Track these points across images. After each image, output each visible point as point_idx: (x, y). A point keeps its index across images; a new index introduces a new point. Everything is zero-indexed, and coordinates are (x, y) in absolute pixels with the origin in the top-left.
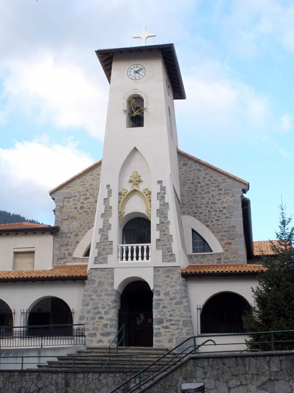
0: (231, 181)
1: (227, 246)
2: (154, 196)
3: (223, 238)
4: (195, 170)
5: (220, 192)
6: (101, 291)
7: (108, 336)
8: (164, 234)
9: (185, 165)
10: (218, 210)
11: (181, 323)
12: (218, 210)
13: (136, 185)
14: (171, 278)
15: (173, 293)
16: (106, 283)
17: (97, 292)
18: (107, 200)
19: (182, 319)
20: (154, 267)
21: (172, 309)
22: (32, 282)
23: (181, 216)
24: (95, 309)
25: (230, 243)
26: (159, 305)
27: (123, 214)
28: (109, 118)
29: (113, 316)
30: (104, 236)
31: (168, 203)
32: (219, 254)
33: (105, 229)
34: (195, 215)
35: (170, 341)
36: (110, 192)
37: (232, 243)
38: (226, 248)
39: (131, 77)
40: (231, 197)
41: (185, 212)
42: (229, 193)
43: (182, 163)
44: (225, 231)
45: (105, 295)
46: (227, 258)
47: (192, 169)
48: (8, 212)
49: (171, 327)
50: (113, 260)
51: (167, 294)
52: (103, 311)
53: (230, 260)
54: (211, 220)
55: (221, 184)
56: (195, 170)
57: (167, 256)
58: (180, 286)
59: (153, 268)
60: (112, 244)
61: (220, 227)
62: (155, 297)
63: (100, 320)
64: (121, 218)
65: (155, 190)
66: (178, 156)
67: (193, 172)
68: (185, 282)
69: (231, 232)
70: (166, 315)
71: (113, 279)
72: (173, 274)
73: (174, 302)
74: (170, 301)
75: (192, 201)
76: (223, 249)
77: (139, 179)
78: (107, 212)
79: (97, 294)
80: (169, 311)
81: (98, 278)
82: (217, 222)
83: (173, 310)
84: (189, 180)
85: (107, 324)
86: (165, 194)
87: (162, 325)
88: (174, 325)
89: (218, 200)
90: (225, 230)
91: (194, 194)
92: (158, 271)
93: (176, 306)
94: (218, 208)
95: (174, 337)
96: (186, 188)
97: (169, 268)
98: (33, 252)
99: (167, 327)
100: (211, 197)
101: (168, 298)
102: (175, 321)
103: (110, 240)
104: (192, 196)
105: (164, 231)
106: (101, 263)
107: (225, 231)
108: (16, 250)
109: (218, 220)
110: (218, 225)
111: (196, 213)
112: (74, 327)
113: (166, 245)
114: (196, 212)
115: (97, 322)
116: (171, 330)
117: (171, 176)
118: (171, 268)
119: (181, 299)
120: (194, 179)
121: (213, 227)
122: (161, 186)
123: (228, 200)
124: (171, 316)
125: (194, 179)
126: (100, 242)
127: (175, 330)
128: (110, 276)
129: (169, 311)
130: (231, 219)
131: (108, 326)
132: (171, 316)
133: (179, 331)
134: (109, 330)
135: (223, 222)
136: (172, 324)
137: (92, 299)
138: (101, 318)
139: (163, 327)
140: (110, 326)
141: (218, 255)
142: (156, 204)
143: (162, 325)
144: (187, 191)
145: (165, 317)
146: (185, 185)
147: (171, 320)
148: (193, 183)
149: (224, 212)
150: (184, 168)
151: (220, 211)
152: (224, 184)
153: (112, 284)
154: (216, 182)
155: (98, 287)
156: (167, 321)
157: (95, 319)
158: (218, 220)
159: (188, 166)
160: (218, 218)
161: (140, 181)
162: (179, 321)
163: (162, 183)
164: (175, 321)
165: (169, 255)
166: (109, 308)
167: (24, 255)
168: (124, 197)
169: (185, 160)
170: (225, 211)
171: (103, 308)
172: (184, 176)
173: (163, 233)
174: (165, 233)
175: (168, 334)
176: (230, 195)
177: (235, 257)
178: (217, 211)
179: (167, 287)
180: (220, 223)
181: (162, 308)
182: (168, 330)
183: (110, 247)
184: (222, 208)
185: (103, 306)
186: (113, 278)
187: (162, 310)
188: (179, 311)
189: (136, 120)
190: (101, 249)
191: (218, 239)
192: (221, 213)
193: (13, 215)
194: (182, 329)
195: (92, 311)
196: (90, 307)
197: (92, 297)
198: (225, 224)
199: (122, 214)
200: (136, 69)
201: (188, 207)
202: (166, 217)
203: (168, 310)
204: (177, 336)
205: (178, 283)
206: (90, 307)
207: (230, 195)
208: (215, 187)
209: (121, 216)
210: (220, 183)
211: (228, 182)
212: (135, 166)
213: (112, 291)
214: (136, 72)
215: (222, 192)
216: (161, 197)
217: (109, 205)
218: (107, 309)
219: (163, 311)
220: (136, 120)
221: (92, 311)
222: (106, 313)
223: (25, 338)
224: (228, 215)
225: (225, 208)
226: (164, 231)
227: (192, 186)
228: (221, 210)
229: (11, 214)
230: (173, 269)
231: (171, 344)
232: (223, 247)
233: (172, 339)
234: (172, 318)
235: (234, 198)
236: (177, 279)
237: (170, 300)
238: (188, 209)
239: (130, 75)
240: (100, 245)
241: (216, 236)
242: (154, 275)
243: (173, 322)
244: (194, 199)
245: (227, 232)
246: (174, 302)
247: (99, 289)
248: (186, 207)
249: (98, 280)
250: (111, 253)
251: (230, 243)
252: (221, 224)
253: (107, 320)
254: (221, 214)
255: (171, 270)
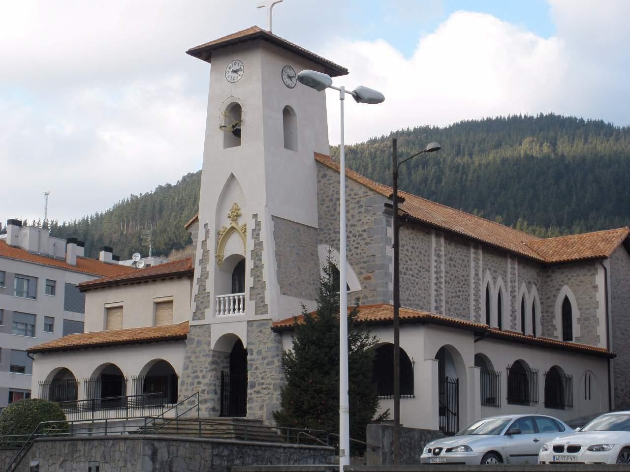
0: (373, 194)
1: (365, 282)
2: (249, 233)
3: (363, 271)
4: (335, 182)
5: (360, 210)
6: (200, 352)
7: (205, 404)
8: (259, 281)
9: (324, 176)
10: (358, 234)
11: (271, 387)
12: (358, 234)
13: (235, 220)
14: (264, 334)
15: (266, 352)
16: (203, 342)
17: (195, 353)
18: (205, 242)
19: (273, 382)
20: (248, 321)
21: (264, 370)
22: (138, 344)
23: (317, 247)
24: (194, 372)
25: (369, 278)
26: (252, 366)
27: (223, 258)
28: (208, 137)
29: (210, 380)
30: (202, 287)
31: (262, 242)
32: (357, 292)
33: (203, 278)
34: (333, 243)
35: (261, 408)
36: (207, 232)
37: (372, 276)
38: (365, 285)
39: (229, 79)
40: (372, 215)
41: (322, 240)
42: (370, 210)
43: (321, 174)
44: (364, 262)
45: (203, 356)
46: (366, 297)
47: (331, 182)
48: (579, 118)
49: (262, 391)
50: (210, 316)
51: (259, 353)
52: (200, 375)
53: (368, 299)
54: (350, 248)
55: (362, 199)
56: (335, 182)
57: (260, 307)
58: (273, 343)
59: (245, 323)
60: (208, 296)
61: (358, 257)
62: (249, 357)
63: (198, 385)
64: (220, 263)
65: (251, 226)
66: (317, 165)
67: (333, 185)
68: (279, 337)
69: (370, 263)
70: (258, 378)
71: (210, 337)
72: (265, 328)
73: (266, 361)
74: (262, 361)
75: (329, 224)
76: (361, 286)
77: (237, 213)
78: (205, 257)
79: (196, 355)
80: (261, 373)
81: (196, 336)
82: (356, 250)
83: (265, 372)
84: (327, 196)
85: (204, 390)
86: (260, 230)
87: (255, 389)
88: (265, 389)
89: (358, 221)
90: (364, 260)
91: (332, 216)
92: (252, 326)
93: (268, 367)
94: (358, 232)
95: (265, 404)
96: (324, 207)
97: (262, 322)
98: (171, 302)
99: (258, 392)
100: (350, 218)
101: (260, 357)
102: (267, 384)
103: (207, 291)
104: (331, 218)
105: (258, 276)
106: (199, 319)
107: (364, 262)
108: (156, 300)
109: (357, 248)
110: (357, 254)
111: (333, 241)
112: (78, 403)
113: (259, 294)
114: (333, 239)
115: (195, 387)
116: (262, 395)
117: (266, 206)
118: (264, 321)
119: (272, 357)
120: (333, 195)
121: (352, 258)
122: (256, 221)
123: (369, 220)
124: (262, 378)
125: (333, 195)
126: (199, 294)
127: (266, 395)
128: (207, 334)
129: (261, 373)
130: (371, 246)
131: (206, 392)
132: (262, 378)
133: (270, 396)
134: (206, 396)
135: (363, 249)
136: (263, 389)
137: (191, 361)
138: (199, 383)
139: (255, 391)
140: (207, 392)
141: (356, 294)
142: (251, 244)
143: (255, 389)
144: (325, 211)
145: (257, 380)
146: (323, 204)
147: (263, 384)
148: (331, 200)
149: (364, 237)
150: (323, 181)
151: (361, 235)
152: (364, 199)
153: (209, 344)
154: (357, 197)
155: (197, 347)
156: (259, 384)
157: (193, 384)
158: (357, 248)
159: (328, 178)
160: (357, 246)
161: (238, 216)
162: (270, 384)
163: (257, 217)
164: (267, 384)
165: (261, 307)
166: (206, 371)
167: (164, 306)
168: (224, 236)
169: (324, 170)
170: (365, 235)
171: (201, 371)
172: (322, 191)
173: (257, 279)
174: (259, 279)
175: (259, 400)
176: (371, 213)
177: (373, 295)
178: (356, 235)
179: (260, 344)
180: (359, 251)
181: (254, 370)
182: (259, 395)
183: (208, 300)
184: (361, 231)
185: (201, 369)
186: (210, 336)
187: (255, 371)
188: (271, 372)
189: (235, 134)
190: (200, 302)
191: (356, 273)
192: (360, 238)
193: (589, 122)
194: (273, 394)
195: (191, 375)
196: (189, 371)
197: (192, 359)
198: (365, 253)
199: (221, 258)
200: (235, 68)
201: (326, 233)
202: (260, 260)
203: (260, 371)
204: (268, 401)
205: (270, 339)
206: (189, 371)
207: (371, 213)
208: (355, 203)
209: (220, 260)
210: (360, 197)
211: (370, 195)
212: (234, 198)
213: (209, 351)
214: (235, 72)
215: (363, 210)
216: (256, 234)
217: (206, 248)
218: (204, 373)
219: (255, 373)
220: (235, 134)
221: (191, 375)
222: (204, 377)
223: (159, 408)
224: (368, 240)
225: (364, 231)
226: (258, 276)
227: (331, 204)
228: (361, 234)
229: (586, 121)
230: (265, 322)
231: (262, 411)
232: (362, 283)
233: (263, 406)
234: (263, 381)
235: (375, 217)
236: (269, 335)
237: (262, 360)
238: (325, 235)
239: (229, 76)
240: (199, 297)
241: (354, 269)
242: (248, 331)
243: (264, 386)
244: (332, 221)
245: (366, 263)
246: (266, 361)
247: (197, 350)
248: (324, 234)
249: (196, 339)
250: (207, 307)
251: (369, 278)
252: (360, 253)
253: (205, 385)
254: (361, 239)
255: (264, 324)
